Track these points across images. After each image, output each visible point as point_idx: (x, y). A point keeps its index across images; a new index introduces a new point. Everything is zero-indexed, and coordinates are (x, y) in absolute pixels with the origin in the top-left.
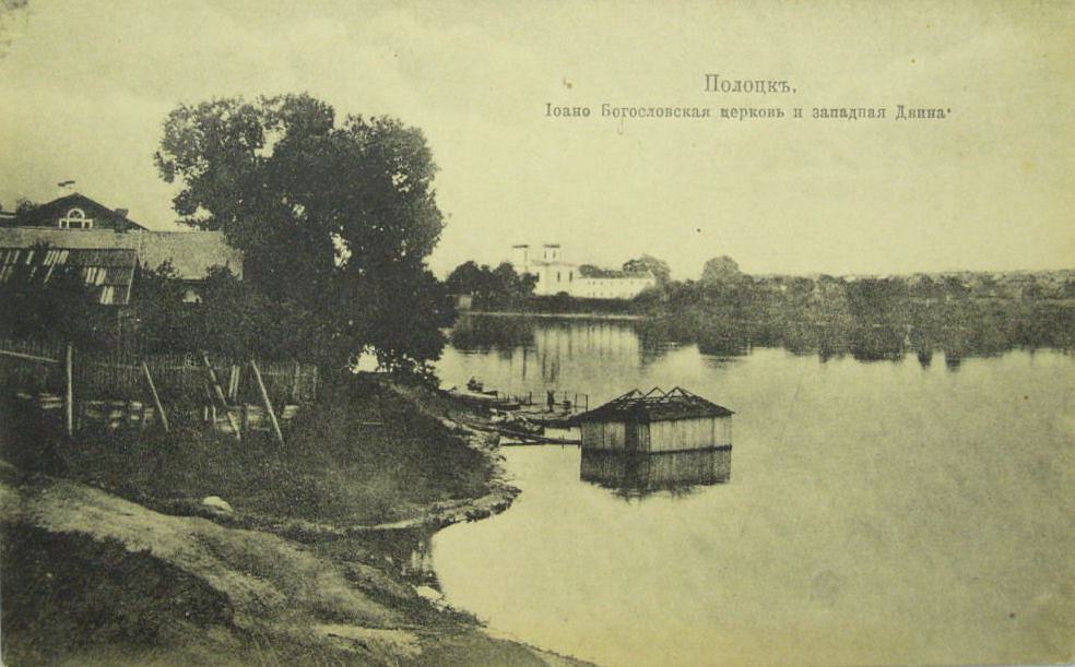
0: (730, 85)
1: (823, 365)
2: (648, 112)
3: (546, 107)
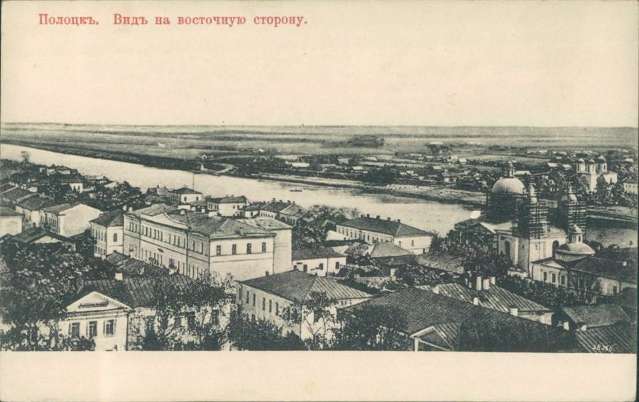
0: (268, 21)
1: (266, 270)
2: (261, 20)
3: (39, 17)
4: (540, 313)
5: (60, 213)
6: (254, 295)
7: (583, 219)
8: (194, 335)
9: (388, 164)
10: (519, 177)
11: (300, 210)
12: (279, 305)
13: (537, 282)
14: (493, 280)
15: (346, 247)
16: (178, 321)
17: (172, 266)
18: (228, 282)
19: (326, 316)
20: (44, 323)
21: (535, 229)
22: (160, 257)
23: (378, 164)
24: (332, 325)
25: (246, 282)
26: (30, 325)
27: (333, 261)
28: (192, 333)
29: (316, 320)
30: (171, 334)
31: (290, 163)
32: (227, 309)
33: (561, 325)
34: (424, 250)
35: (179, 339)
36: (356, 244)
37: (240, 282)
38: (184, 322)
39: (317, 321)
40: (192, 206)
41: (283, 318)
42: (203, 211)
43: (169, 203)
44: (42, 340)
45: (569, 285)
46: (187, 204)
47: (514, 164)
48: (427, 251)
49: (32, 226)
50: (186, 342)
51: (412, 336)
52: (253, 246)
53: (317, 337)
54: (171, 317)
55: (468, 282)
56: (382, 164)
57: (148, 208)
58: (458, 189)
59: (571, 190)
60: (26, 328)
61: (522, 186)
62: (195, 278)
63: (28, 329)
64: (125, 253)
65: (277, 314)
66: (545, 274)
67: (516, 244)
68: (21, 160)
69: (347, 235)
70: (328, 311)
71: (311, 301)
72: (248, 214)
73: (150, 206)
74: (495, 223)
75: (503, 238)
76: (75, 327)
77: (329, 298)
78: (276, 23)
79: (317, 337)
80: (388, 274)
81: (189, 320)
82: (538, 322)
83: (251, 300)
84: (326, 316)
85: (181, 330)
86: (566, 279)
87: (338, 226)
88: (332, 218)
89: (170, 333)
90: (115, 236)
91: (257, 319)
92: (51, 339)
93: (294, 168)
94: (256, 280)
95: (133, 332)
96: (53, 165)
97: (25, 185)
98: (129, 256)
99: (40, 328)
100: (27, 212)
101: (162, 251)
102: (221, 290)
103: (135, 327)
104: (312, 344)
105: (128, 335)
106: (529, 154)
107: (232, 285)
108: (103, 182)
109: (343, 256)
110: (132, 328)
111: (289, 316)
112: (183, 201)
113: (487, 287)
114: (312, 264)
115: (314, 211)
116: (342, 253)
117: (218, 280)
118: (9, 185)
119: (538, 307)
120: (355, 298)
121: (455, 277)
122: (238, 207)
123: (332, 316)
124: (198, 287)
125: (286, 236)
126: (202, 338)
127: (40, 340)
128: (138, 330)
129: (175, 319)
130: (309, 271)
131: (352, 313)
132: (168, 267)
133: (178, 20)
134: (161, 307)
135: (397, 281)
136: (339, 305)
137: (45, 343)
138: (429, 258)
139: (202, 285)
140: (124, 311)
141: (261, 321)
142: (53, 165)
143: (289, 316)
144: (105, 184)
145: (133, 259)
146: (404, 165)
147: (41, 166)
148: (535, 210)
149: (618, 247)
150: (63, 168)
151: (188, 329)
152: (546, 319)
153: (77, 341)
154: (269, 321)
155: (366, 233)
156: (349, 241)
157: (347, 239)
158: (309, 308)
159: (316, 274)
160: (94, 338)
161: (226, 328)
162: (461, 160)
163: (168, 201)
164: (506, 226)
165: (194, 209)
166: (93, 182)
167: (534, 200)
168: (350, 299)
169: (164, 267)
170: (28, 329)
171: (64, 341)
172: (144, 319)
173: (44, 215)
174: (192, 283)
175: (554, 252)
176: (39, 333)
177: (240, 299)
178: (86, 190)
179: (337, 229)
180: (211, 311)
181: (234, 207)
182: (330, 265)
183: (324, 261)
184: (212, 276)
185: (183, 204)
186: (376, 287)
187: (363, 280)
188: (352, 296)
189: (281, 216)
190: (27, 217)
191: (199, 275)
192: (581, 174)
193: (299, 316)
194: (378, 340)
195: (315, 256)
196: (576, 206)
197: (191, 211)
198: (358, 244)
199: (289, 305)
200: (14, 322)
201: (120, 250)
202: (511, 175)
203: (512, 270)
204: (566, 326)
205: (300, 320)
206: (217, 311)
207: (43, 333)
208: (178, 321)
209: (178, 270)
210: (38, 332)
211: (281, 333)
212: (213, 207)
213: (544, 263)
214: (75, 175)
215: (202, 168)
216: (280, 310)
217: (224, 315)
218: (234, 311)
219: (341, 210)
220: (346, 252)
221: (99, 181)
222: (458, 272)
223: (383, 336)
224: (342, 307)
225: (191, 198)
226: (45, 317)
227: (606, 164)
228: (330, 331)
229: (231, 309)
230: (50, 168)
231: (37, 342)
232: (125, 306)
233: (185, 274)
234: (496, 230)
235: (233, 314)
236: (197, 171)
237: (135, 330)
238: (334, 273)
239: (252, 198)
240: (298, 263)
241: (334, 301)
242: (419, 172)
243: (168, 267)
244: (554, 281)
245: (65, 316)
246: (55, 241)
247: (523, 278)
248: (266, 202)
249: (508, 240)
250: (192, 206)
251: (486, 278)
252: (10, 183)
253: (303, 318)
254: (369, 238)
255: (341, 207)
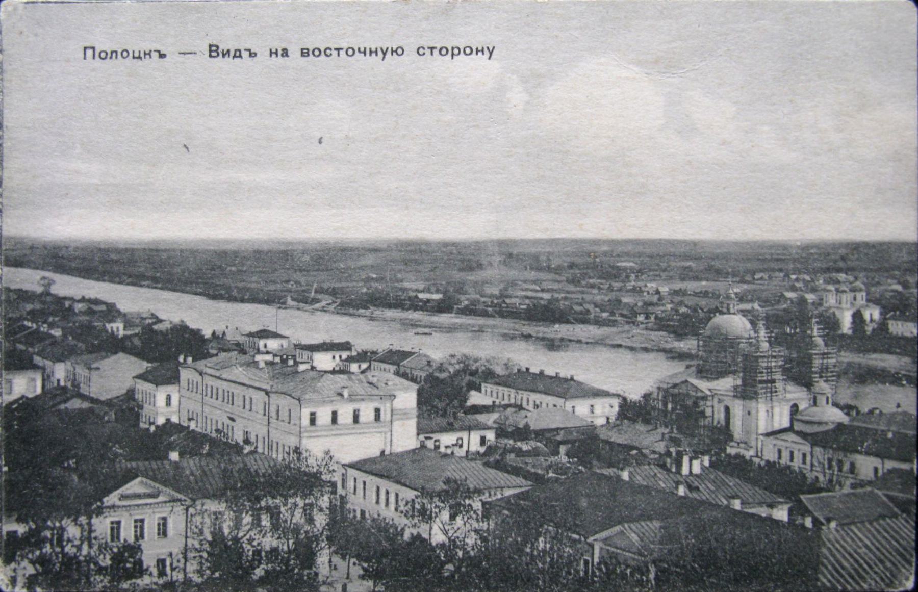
4: (771, 506)
5: (94, 366)
6: (364, 483)
7: (832, 372)
8: (279, 538)
9: (556, 295)
10: (744, 313)
11: (429, 362)
12: (400, 498)
13: (768, 462)
14: (706, 461)
15: (495, 416)
16: (257, 523)
17: (247, 441)
18: (326, 464)
19: (467, 512)
20: (72, 521)
21: (766, 388)
22: (230, 428)
23: (540, 295)
24: (475, 525)
25: (353, 466)
26: (54, 524)
27: (475, 437)
28: (277, 536)
29: (453, 517)
30: (248, 537)
31: (414, 294)
32: (325, 501)
33: (801, 521)
34: (608, 419)
35: (259, 544)
36: (510, 410)
37: (344, 465)
38: (266, 521)
39: (454, 519)
40: (275, 355)
41: (406, 515)
42: (291, 362)
43: (243, 352)
44: (70, 545)
45: (812, 465)
46: (268, 353)
47: (736, 294)
48: (612, 419)
49: (55, 384)
50: (268, 548)
51: (590, 540)
52: (361, 413)
53: (454, 541)
54: (247, 513)
55: (671, 464)
56: (547, 296)
57: (214, 359)
58: (659, 330)
59: (815, 331)
60: (48, 528)
61: (749, 326)
62: (280, 458)
63: (52, 529)
64: (182, 423)
65: (396, 510)
66: (780, 451)
67: (737, 408)
68: (39, 290)
69: (497, 398)
70: (470, 505)
71: (446, 492)
72: (354, 367)
73: (217, 355)
74: (709, 379)
75: (720, 401)
76: (116, 527)
77: (471, 486)
78: (453, 55)
79: (454, 541)
80: (557, 453)
81: (271, 518)
82: (769, 519)
83: (360, 491)
84: (467, 512)
85: (261, 531)
86: (808, 458)
87: (483, 385)
88: (474, 373)
89: (245, 535)
90: (169, 398)
91: (367, 515)
92: (81, 544)
93: (421, 300)
94: (365, 461)
95: (193, 533)
96: (83, 298)
97: (45, 326)
98: (189, 427)
99: (67, 529)
100: (48, 363)
101: (232, 419)
102: (316, 476)
103: (196, 527)
104: (446, 552)
105: (186, 537)
106: (758, 280)
107: (331, 469)
108: (150, 321)
109: (489, 428)
110: (193, 527)
111: (413, 511)
112: (262, 348)
113: (696, 469)
114: (448, 439)
115: (450, 364)
116: (490, 423)
117: (311, 461)
118: (23, 326)
119: (769, 497)
120: (509, 487)
121: (652, 456)
122: (340, 357)
123: (475, 512)
124: (285, 471)
125: (407, 398)
126: (291, 542)
127: (67, 544)
128: (201, 532)
129: (252, 515)
130: (442, 450)
131: (504, 508)
132: (242, 443)
133: (289, 54)
134: (233, 502)
135: (569, 462)
136: (485, 497)
137: (74, 550)
138: (615, 430)
139: (290, 469)
140: (183, 505)
141: (374, 520)
142: (83, 298)
143: (413, 511)
144: (155, 323)
145: (193, 431)
146: (580, 296)
147: (65, 298)
148: (766, 360)
149: (881, 412)
150: (97, 302)
151: (271, 530)
152: (781, 514)
153: (117, 546)
154: (385, 519)
155: (525, 395)
156: (500, 406)
157: (497, 403)
158: (443, 502)
159: (453, 453)
160: (141, 542)
161: (324, 528)
162: (661, 289)
163: (240, 349)
164: (726, 384)
165: (278, 360)
166: (137, 321)
167: (765, 346)
168: (502, 488)
169: (237, 443)
170: (52, 529)
171: (100, 546)
172: (209, 516)
173: (71, 369)
174: (275, 465)
175: (792, 421)
176: (65, 537)
177: (343, 487)
178: (129, 333)
179: (483, 389)
180: (303, 505)
181: (334, 357)
182: (473, 442)
183: (464, 435)
184: (304, 456)
185: (263, 353)
186: (539, 472)
187: (519, 462)
188: (510, 485)
189: (402, 370)
190: (48, 371)
191: (286, 455)
192: (830, 308)
193: (428, 513)
194: (541, 545)
195: (450, 428)
196: (824, 354)
197: (696, 571)
198: (513, 410)
199: (414, 497)
200: (33, 521)
201: (175, 419)
202: (732, 311)
203: (732, 447)
204: (808, 522)
205: (430, 518)
206: (311, 505)
207: (71, 536)
208: (257, 523)
209: (256, 447)
210: (66, 533)
211: (402, 535)
212: (305, 357)
213: (778, 436)
214: (111, 312)
215: (290, 302)
216: (402, 504)
217: (321, 510)
218: (335, 505)
219: (488, 361)
220: (495, 422)
221: (145, 319)
222: (657, 449)
223: (548, 539)
224: (489, 500)
225: (273, 344)
226: (74, 515)
227: (864, 294)
228: (473, 533)
229: (331, 502)
230: (79, 301)
231: (63, 547)
232: (183, 498)
233: (266, 453)
234: (710, 390)
235: (332, 508)
236: (282, 304)
237: (196, 530)
238: (478, 453)
239: (361, 344)
240: (427, 438)
241: (479, 492)
242: (601, 307)
243: (242, 443)
244: (792, 459)
245: (99, 512)
246: (86, 405)
247: (748, 458)
248: (380, 350)
249: (726, 403)
250: (275, 355)
251: (696, 458)
252: (26, 323)
253: (434, 515)
254: (528, 401)
255: (488, 357)
